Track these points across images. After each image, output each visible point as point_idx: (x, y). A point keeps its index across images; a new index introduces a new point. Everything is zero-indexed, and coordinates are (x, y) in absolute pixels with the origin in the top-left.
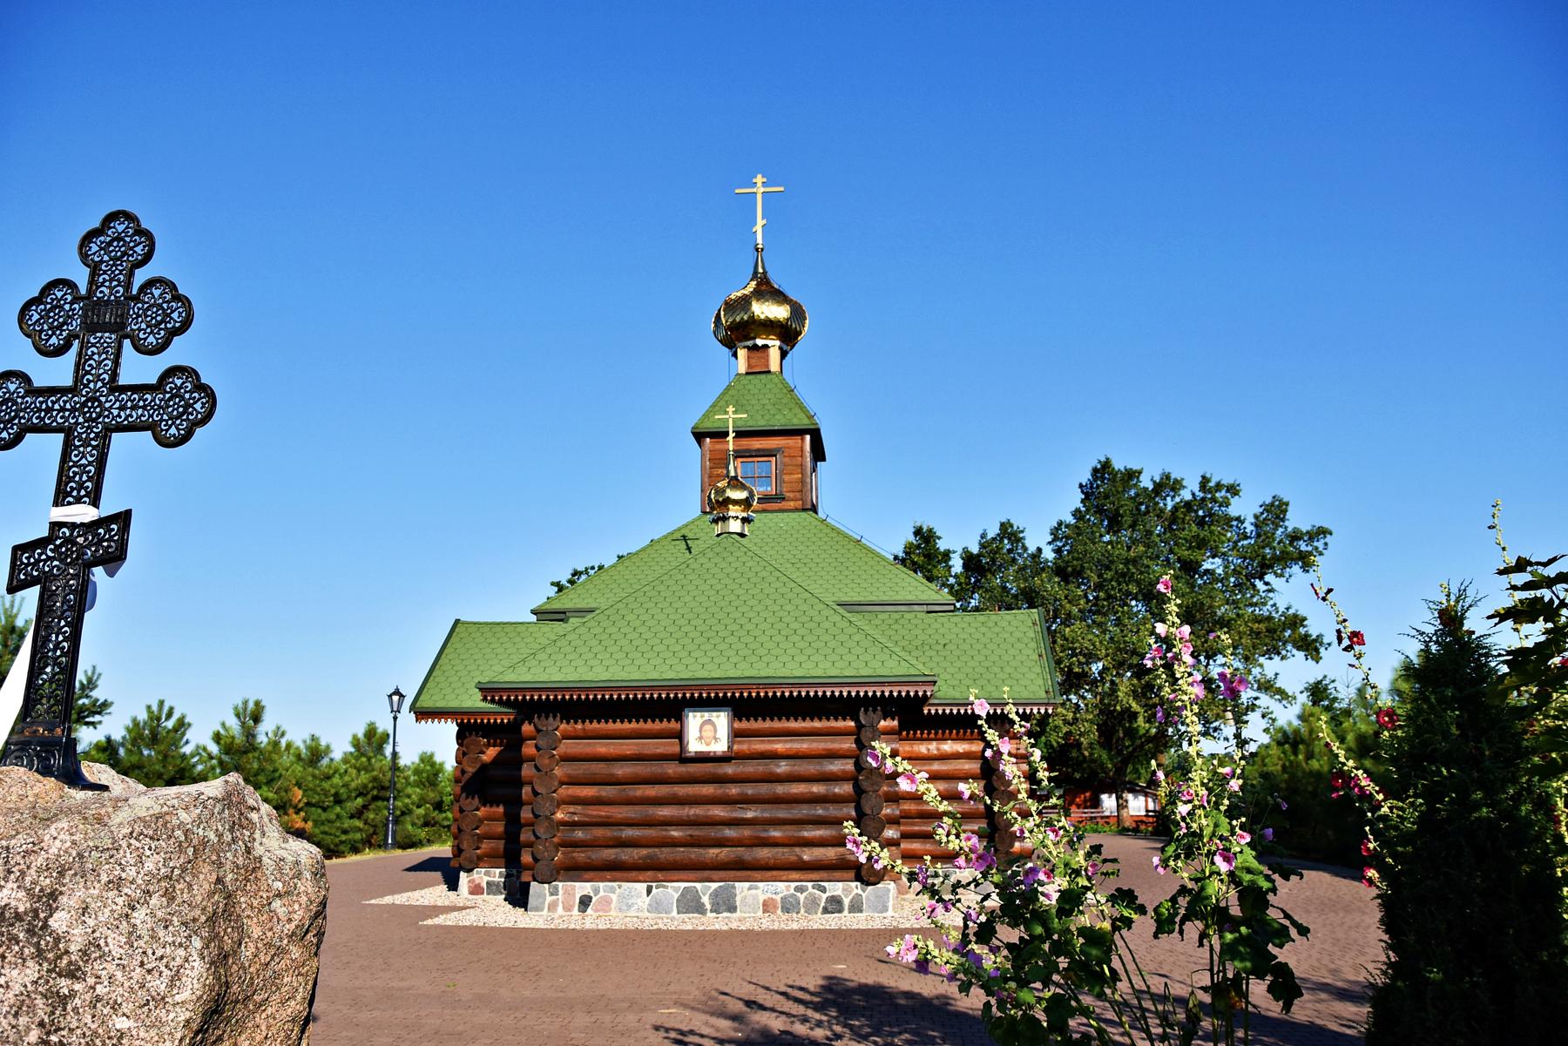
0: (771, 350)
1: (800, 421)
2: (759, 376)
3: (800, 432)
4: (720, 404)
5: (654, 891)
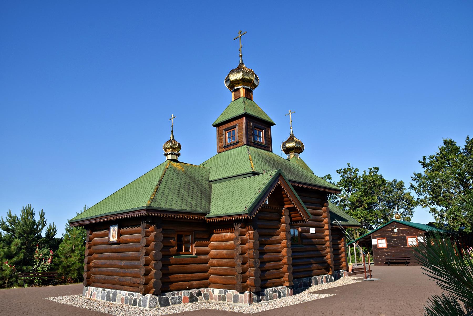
5: (103, 291)
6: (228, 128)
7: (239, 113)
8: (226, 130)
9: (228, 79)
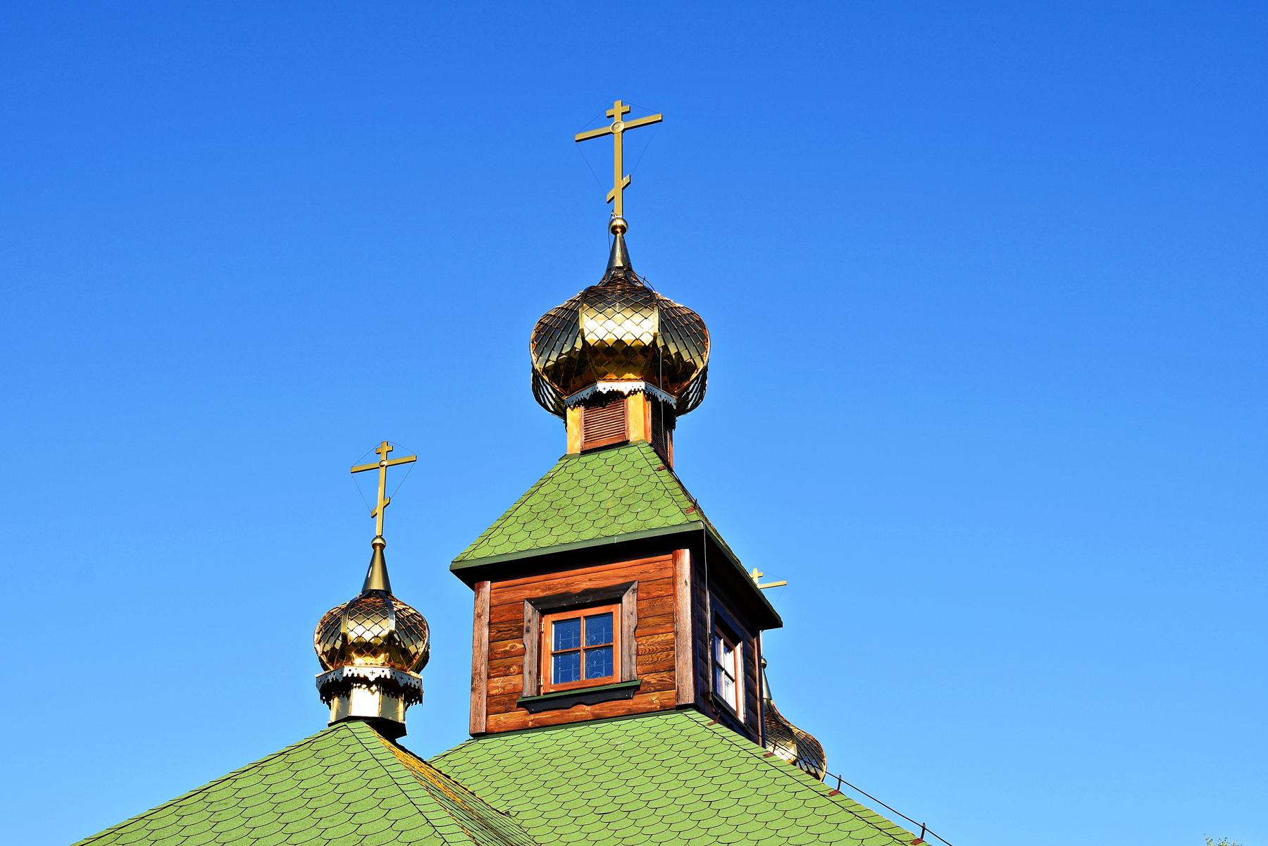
0: (631, 401)
1: (671, 518)
2: (604, 455)
3: (664, 544)
4: (517, 513)
6: (566, 596)
7: (544, 542)
8: (546, 606)
9: (566, 322)
